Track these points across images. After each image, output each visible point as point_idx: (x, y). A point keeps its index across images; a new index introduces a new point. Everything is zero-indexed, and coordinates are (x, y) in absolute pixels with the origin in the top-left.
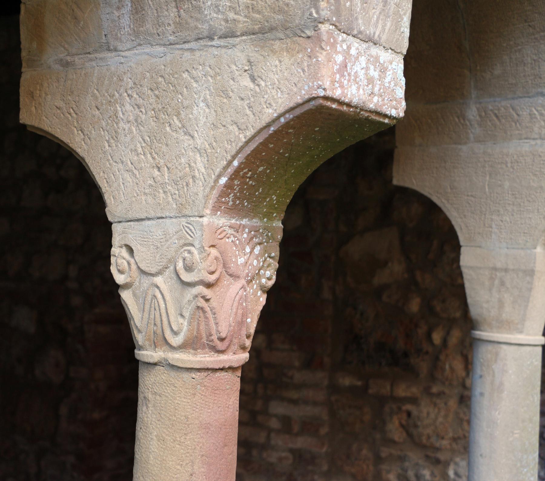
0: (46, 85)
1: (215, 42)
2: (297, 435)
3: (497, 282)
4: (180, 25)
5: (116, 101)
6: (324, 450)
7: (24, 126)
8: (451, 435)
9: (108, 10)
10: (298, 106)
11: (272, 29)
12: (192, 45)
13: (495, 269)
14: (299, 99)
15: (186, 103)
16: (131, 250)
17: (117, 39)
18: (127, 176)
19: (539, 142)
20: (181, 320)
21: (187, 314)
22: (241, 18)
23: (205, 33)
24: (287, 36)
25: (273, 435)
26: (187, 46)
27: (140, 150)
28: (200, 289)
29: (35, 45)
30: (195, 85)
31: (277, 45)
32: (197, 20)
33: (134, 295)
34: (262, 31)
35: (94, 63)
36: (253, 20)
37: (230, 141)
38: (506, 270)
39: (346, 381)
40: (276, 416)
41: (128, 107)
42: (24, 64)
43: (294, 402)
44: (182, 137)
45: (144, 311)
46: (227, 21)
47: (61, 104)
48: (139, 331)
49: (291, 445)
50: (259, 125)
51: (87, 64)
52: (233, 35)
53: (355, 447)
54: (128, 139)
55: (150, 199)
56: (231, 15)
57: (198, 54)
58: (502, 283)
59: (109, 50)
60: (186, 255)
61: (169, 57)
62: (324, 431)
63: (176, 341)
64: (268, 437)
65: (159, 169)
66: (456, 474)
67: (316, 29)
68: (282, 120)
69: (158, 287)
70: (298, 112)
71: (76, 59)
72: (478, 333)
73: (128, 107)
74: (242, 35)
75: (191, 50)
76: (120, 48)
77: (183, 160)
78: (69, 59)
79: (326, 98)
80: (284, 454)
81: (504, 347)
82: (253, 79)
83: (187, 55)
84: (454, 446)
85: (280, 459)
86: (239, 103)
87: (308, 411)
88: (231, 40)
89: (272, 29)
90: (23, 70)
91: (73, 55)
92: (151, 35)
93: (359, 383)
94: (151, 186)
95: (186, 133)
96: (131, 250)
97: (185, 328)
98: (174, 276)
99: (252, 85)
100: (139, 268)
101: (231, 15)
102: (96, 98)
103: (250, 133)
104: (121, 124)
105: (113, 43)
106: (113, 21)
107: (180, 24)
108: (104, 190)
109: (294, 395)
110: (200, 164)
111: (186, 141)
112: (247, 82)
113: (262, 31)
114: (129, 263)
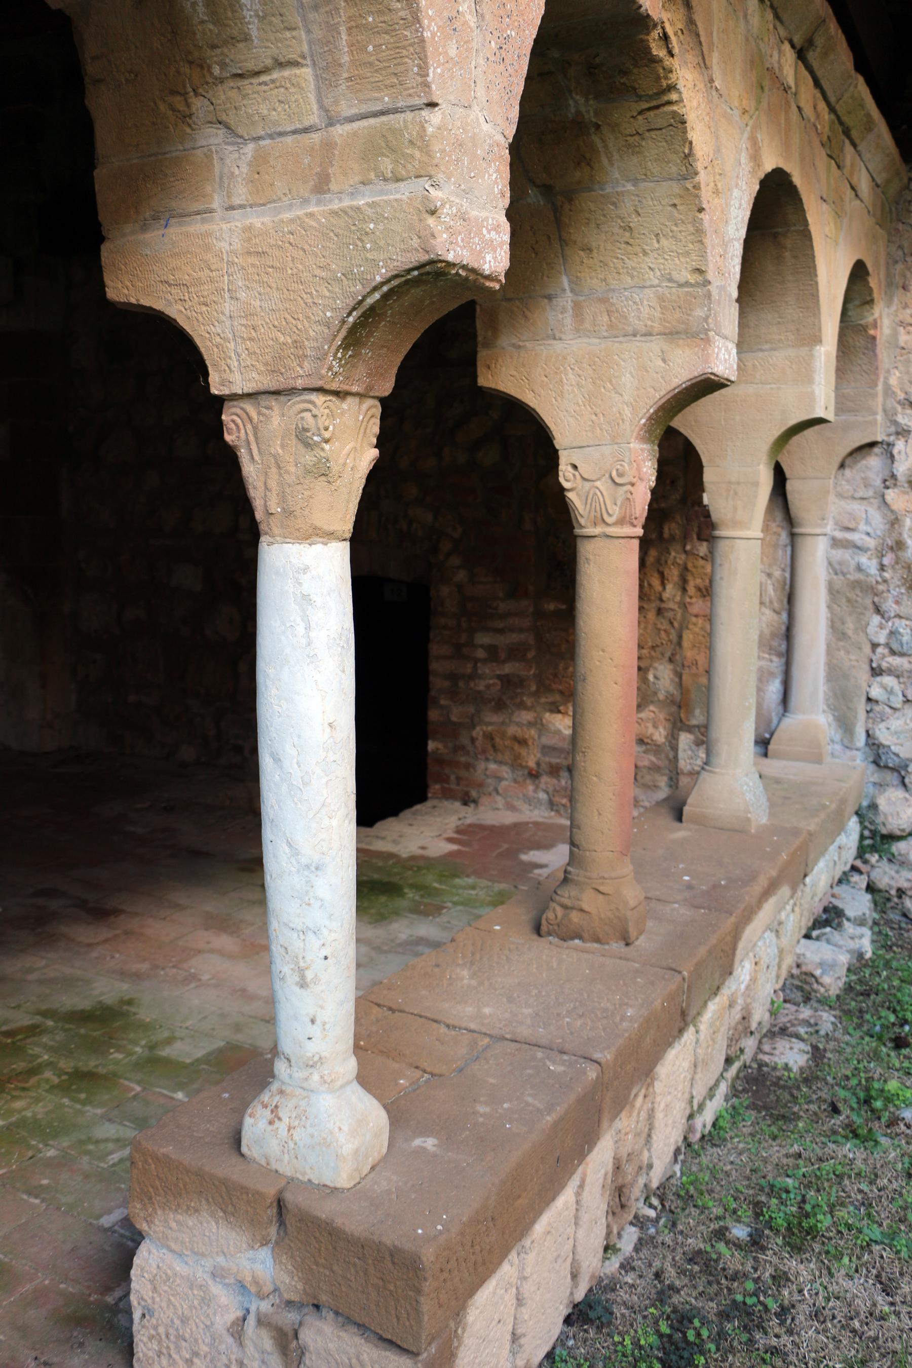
0: (500, 360)
1: (638, 338)
2: (504, 662)
3: (732, 492)
4: (611, 326)
5: (561, 372)
6: (532, 672)
7: (481, 388)
8: (650, 644)
9: (553, 313)
10: (696, 377)
11: (677, 333)
12: (621, 339)
13: (730, 483)
14: (696, 374)
15: (616, 374)
16: (575, 467)
17: (561, 332)
18: (571, 420)
19: (760, 386)
20: (614, 507)
21: (619, 503)
22: (656, 325)
23: (631, 333)
24: (688, 337)
25: (479, 665)
26: (616, 339)
27: (581, 403)
28: (629, 487)
29: (490, 333)
30: (622, 363)
31: (681, 342)
32: (624, 324)
33: (578, 494)
34: (671, 333)
35: (542, 347)
36: (665, 327)
37: (648, 398)
38: (738, 483)
39: (551, 606)
40: (482, 646)
41: (571, 376)
42: (479, 346)
43: (500, 631)
44: (613, 395)
45: (586, 503)
46: (646, 326)
47: (515, 373)
48: (582, 516)
49: (498, 672)
50: (669, 388)
51: (537, 348)
52: (651, 335)
53: (561, 666)
54: (571, 396)
55: (589, 434)
56: (649, 323)
57: (625, 345)
58: (736, 493)
59: (555, 339)
60: (619, 467)
61: (603, 346)
62: (530, 655)
63: (609, 520)
64: (475, 668)
65: (596, 415)
66: (656, 677)
67: (706, 334)
68: (684, 386)
69: (598, 488)
70: (694, 381)
71: (527, 344)
72: (717, 533)
73: (571, 376)
74: (657, 335)
75: (620, 342)
76: (563, 337)
77: (614, 409)
78: (521, 343)
79: (712, 373)
80: (491, 682)
81: (738, 541)
82: (664, 361)
83: (617, 345)
84: (653, 653)
85: (488, 687)
86: (655, 375)
87: (514, 638)
88: (650, 338)
89: (677, 333)
90: (478, 349)
91: (524, 341)
92: (589, 331)
93: (564, 607)
94: (590, 426)
95: (617, 393)
96: (575, 467)
97: (617, 512)
98: (610, 481)
99: (663, 365)
100: (582, 477)
101: (649, 323)
102: (545, 370)
103: (662, 393)
104: (566, 387)
105: (558, 335)
106: (558, 321)
107: (611, 326)
108: (552, 429)
109: (500, 624)
110: (627, 412)
111: (617, 398)
112: (660, 363)
113: (671, 333)
114: (574, 475)
